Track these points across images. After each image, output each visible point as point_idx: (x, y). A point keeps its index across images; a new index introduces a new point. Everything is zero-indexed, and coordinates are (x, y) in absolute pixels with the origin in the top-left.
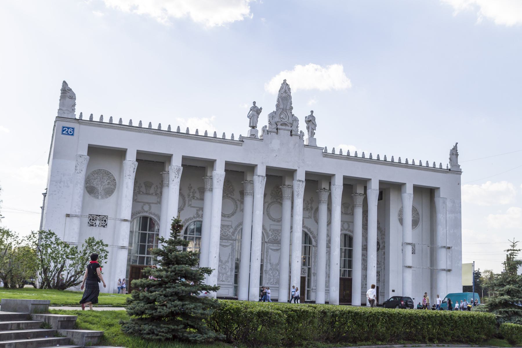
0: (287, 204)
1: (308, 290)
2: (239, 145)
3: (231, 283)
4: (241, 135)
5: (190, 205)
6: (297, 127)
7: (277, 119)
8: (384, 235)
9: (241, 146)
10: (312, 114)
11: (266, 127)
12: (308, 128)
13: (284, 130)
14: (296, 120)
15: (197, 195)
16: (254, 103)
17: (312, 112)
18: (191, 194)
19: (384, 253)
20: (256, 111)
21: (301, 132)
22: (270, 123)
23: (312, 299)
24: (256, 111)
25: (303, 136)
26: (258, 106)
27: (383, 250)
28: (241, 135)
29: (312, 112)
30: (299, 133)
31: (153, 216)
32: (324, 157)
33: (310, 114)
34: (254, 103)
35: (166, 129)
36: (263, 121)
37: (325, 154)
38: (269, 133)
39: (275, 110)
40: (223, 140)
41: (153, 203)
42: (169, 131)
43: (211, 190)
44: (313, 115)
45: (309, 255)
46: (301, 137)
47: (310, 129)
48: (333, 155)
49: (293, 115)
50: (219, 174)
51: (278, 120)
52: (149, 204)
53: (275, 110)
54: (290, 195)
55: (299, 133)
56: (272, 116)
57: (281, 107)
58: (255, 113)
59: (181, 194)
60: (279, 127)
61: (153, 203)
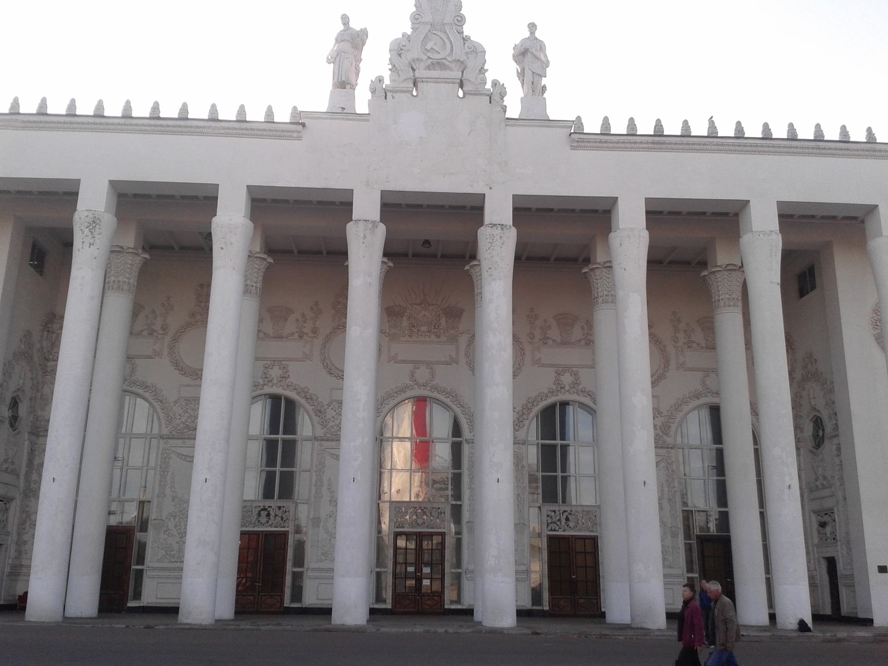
0: (729, 322)
1: (294, 573)
2: (290, 138)
3: (150, 573)
4: (295, 108)
5: (537, 362)
6: (482, 71)
7: (415, 53)
8: (831, 391)
9: (299, 138)
10: (532, 33)
11: (380, 80)
12: (521, 75)
13: (437, 80)
14: (477, 52)
15: (699, 337)
16: (345, 20)
17: (532, 27)
18: (681, 335)
19: (839, 449)
20: (352, 42)
21: (495, 83)
22: (394, 69)
23: (310, 599)
24: (352, 42)
25: (503, 95)
26: (356, 25)
27: (835, 441)
28: (295, 108)
29: (532, 27)
30: (488, 86)
31: (292, 395)
32: (573, 148)
33: (342, 27)
34: (345, 20)
35: (862, 138)
36: (375, 64)
37: (576, 136)
38: (389, 95)
39: (409, 31)
40: (685, 140)
41: (438, 363)
42: (713, 134)
43: (612, 299)
44: (538, 34)
45: (564, 469)
46: (496, 97)
47: (528, 73)
48: (605, 140)
49: (466, 39)
50: (630, 248)
51: (416, 56)
52: (429, 364)
53: (409, 31)
54: (738, 294)
55: (488, 86)
56: (398, 50)
57: (428, 18)
58: (347, 46)
59: (654, 339)
60: (420, 73)
61: (438, 363)
